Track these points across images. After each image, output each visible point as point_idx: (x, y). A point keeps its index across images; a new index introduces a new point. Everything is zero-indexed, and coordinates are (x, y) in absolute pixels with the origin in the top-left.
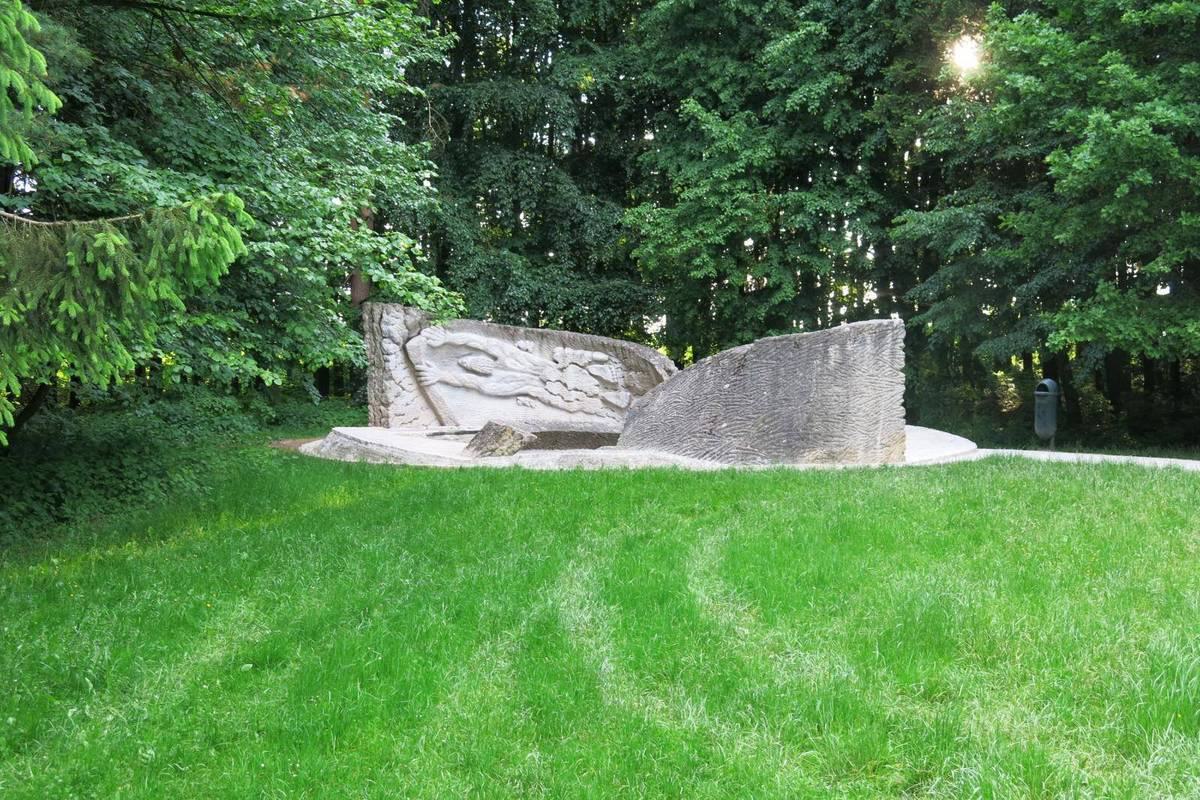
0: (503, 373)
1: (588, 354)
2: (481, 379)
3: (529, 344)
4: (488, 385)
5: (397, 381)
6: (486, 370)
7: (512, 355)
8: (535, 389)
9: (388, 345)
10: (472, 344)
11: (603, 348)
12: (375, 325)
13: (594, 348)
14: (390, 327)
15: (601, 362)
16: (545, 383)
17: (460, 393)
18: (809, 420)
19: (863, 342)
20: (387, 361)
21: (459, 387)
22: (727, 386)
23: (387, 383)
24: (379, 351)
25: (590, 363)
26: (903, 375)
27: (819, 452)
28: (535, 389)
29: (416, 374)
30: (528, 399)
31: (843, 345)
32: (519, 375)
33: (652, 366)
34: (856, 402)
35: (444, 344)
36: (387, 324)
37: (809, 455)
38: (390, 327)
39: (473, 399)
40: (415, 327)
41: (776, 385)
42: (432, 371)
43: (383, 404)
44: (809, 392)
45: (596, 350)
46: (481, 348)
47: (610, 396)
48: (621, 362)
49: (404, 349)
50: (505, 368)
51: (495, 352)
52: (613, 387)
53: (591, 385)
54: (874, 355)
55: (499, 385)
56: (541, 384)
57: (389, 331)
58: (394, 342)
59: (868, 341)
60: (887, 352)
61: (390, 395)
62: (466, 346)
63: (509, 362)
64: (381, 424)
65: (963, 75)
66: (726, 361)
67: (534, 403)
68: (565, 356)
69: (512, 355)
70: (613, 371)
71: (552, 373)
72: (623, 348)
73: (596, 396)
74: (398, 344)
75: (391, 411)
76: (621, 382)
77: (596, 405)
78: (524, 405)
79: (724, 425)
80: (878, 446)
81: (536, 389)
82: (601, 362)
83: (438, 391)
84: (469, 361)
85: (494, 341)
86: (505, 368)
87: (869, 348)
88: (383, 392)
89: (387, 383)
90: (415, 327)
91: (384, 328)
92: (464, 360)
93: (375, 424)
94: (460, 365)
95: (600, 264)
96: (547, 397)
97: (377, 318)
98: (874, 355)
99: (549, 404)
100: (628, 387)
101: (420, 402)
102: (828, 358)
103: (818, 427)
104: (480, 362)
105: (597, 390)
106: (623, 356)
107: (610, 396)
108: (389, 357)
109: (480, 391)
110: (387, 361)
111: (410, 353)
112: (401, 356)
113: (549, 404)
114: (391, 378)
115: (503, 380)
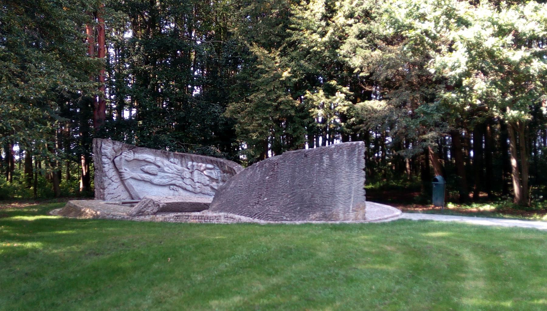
0: (163, 174)
1: (204, 165)
3: (176, 161)
4: (156, 180)
5: (110, 177)
7: (167, 166)
9: (105, 160)
10: (147, 160)
11: (211, 162)
13: (207, 162)
14: (106, 151)
16: (183, 179)
17: (142, 184)
18: (312, 197)
19: (342, 154)
22: (268, 177)
23: (103, 178)
24: (100, 163)
25: (205, 170)
26: (364, 172)
27: (318, 214)
29: (120, 174)
30: (175, 187)
31: (331, 156)
32: (170, 175)
33: (234, 171)
34: (338, 187)
35: (134, 159)
36: (104, 149)
37: (312, 216)
38: (106, 151)
40: (119, 151)
41: (293, 178)
42: (128, 172)
43: (102, 188)
44: (312, 181)
45: (208, 163)
46: (152, 161)
48: (220, 169)
49: (113, 162)
50: (164, 172)
51: (159, 164)
52: (217, 181)
53: (206, 180)
54: (348, 161)
55: (161, 180)
56: (182, 180)
58: (108, 158)
59: (345, 153)
60: (355, 159)
61: (106, 184)
63: (166, 169)
64: (101, 198)
66: (267, 165)
67: (177, 189)
68: (193, 166)
69: (167, 166)
70: (215, 174)
72: (221, 162)
73: (208, 185)
74: (110, 159)
75: (106, 192)
76: (220, 179)
78: (173, 189)
79: (266, 199)
80: (351, 211)
81: (179, 182)
84: (146, 168)
85: (158, 158)
86: (164, 172)
87: (345, 157)
88: (102, 182)
89: (103, 178)
90: (119, 151)
91: (103, 151)
92: (143, 167)
93: (98, 199)
94: (142, 170)
95: (387, 238)
96: (184, 186)
97: (99, 146)
98: (348, 161)
99: (185, 189)
101: (122, 188)
102: (323, 162)
103: (318, 200)
105: (208, 183)
106: (221, 166)
108: (105, 166)
109: (151, 183)
110: (104, 167)
111: (116, 163)
112: (111, 165)
114: (106, 176)
115: (163, 177)
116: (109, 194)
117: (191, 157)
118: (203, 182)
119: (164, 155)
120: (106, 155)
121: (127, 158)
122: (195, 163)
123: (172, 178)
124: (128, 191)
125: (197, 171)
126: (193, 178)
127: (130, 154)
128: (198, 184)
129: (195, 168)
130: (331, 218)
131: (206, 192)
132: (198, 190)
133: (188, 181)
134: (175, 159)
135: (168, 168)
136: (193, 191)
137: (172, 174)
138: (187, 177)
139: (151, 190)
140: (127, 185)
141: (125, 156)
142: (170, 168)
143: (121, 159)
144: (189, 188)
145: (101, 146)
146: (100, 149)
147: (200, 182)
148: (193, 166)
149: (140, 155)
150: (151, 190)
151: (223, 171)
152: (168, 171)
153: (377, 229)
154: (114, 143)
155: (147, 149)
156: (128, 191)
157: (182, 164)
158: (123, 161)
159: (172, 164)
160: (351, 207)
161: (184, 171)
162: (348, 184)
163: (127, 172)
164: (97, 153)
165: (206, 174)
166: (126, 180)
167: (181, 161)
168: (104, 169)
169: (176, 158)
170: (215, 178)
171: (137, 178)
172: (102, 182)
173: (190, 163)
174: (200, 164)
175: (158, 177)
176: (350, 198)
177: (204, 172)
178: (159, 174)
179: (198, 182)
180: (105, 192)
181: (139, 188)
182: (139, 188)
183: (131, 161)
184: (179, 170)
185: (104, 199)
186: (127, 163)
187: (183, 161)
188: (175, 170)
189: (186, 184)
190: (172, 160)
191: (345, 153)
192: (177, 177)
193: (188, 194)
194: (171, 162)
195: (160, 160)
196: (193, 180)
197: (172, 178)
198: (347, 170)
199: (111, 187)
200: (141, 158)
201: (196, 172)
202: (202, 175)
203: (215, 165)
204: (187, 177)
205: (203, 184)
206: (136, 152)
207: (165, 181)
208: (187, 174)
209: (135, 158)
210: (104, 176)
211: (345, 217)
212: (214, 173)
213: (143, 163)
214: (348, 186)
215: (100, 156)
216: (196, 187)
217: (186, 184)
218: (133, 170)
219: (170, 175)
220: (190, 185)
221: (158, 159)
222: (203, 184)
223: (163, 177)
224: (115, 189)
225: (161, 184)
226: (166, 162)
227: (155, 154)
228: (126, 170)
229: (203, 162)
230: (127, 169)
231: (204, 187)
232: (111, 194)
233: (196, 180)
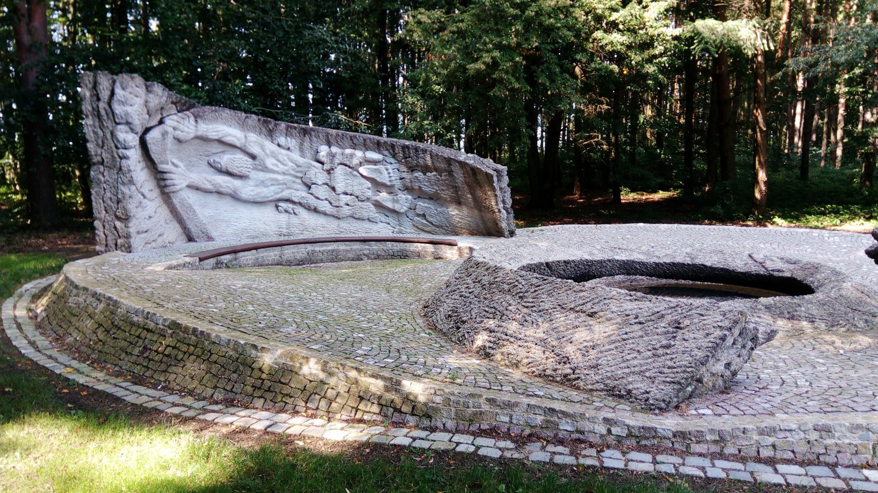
0: (262, 175)
1: (359, 154)
2: (237, 183)
3: (292, 143)
4: (247, 190)
6: (244, 171)
7: (273, 155)
8: (298, 193)
10: (228, 139)
11: (378, 147)
12: (102, 105)
14: (129, 109)
15: (375, 162)
17: (212, 199)
20: (126, 158)
21: (211, 192)
23: (125, 189)
25: (361, 164)
28: (298, 193)
32: (280, 177)
36: (123, 103)
38: (129, 109)
39: (226, 209)
43: (119, 218)
46: (238, 144)
47: (383, 197)
50: (265, 169)
51: (255, 150)
52: (390, 189)
53: (365, 188)
55: (259, 190)
56: (305, 188)
57: (127, 114)
61: (131, 206)
62: (220, 142)
63: (270, 162)
65: (101, 76)
68: (332, 156)
71: (318, 175)
77: (370, 210)
78: (286, 211)
81: (299, 194)
82: (375, 162)
83: (186, 198)
84: (226, 159)
85: (253, 137)
86: (265, 169)
89: (125, 189)
91: (118, 109)
96: (313, 202)
97: (105, 94)
99: (316, 210)
100: (408, 189)
101: (164, 212)
104: (229, 159)
105: (369, 193)
107: (383, 197)
109: (235, 197)
110: (126, 158)
113: (316, 210)
115: (263, 183)
116: (138, 233)
117: (327, 135)
118: (357, 193)
119: (264, 129)
120: (128, 123)
121: (178, 134)
124: (181, 221)
125: (340, 166)
126: (334, 184)
127: (186, 122)
128: (345, 199)
129: (337, 161)
131: (365, 215)
132: (346, 210)
133: (322, 192)
134: (289, 139)
137: (284, 174)
138: (320, 183)
140: (178, 206)
141: (175, 129)
143: (164, 134)
144: (324, 206)
145: (113, 93)
146: (109, 104)
147: (349, 192)
148: (332, 156)
149: (210, 127)
150: (235, 216)
151: (409, 168)
152: (275, 168)
153: (303, 256)
154: (148, 90)
155: (227, 111)
156: (181, 221)
157: (301, 150)
158: (170, 140)
159: (284, 152)
161: (309, 167)
163: (180, 170)
164: (99, 116)
165: (365, 174)
166: (178, 191)
167: (301, 144)
168: (124, 162)
169: (291, 136)
170: (389, 184)
171: (203, 186)
172: (119, 201)
173: (324, 150)
175: (251, 182)
177: (361, 170)
178: (253, 174)
179: (346, 194)
180: (131, 230)
181: (208, 212)
182: (208, 212)
183: (186, 141)
184: (298, 166)
185: (129, 249)
186: (176, 147)
187: (307, 144)
188: (291, 164)
189: (318, 198)
192: (294, 182)
193: (321, 220)
194: (279, 145)
195: (255, 141)
196: (334, 189)
200: (213, 135)
201: (340, 171)
202: (354, 175)
203: (386, 153)
204: (320, 183)
205: (357, 197)
206: (201, 117)
207: (270, 192)
208: (318, 174)
209: (199, 133)
210: (123, 184)
212: (386, 172)
213: (216, 148)
215: (109, 124)
216: (342, 204)
217: (318, 198)
218: (190, 166)
220: (326, 199)
221: (254, 139)
222: (357, 197)
223: (263, 183)
224: (150, 217)
225: (259, 200)
226: (270, 146)
227: (243, 126)
229: (354, 147)
231: (360, 203)
232: (143, 232)
233: (340, 188)
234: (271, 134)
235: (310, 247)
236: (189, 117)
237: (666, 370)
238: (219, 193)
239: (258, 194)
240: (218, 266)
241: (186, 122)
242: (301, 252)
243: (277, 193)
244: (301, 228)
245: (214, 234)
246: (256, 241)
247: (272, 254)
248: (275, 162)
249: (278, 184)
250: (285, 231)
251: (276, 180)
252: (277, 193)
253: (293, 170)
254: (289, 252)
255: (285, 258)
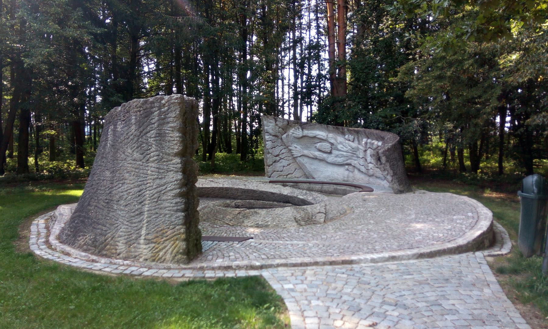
3: (351, 137)
17: (316, 162)
26: (177, 160)
32: (345, 153)
51: (332, 141)
55: (336, 159)
59: (133, 121)
63: (340, 147)
69: (341, 143)
80: (142, 241)
85: (331, 135)
115: (337, 156)
122: (369, 141)
123: (347, 157)
127: (297, 131)
129: (368, 146)
130: (103, 249)
132: (371, 172)
134: (350, 136)
135: (342, 146)
136: (367, 173)
138: (361, 157)
139: (325, 169)
141: (293, 133)
142: (344, 146)
144: (363, 169)
148: (366, 143)
149: (309, 132)
150: (325, 169)
152: (342, 149)
159: (347, 141)
160: (143, 232)
162: (136, 184)
174: (374, 141)
176: (141, 213)
181: (313, 167)
182: (313, 167)
188: (349, 147)
190: (347, 136)
191: (133, 121)
197: (347, 157)
198: (136, 155)
199: (279, 166)
200: (311, 135)
206: (305, 128)
207: (340, 160)
209: (304, 135)
211: (130, 252)
214: (136, 189)
219: (345, 153)
223: (337, 156)
228: (296, 147)
230: (298, 147)
234: (343, 134)
235: (335, 186)
236: (299, 129)
237: (244, 255)
238: (316, 159)
239: (336, 160)
240: (284, 186)
241: (297, 131)
242: (332, 188)
243: (344, 161)
244: (353, 178)
245: (315, 176)
246: (333, 181)
247: (318, 187)
248: (343, 146)
249: (345, 157)
250: (346, 179)
251: (342, 155)
252: (344, 161)
253: (351, 150)
254: (326, 187)
255: (323, 189)
